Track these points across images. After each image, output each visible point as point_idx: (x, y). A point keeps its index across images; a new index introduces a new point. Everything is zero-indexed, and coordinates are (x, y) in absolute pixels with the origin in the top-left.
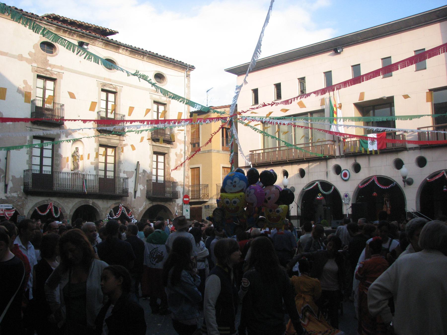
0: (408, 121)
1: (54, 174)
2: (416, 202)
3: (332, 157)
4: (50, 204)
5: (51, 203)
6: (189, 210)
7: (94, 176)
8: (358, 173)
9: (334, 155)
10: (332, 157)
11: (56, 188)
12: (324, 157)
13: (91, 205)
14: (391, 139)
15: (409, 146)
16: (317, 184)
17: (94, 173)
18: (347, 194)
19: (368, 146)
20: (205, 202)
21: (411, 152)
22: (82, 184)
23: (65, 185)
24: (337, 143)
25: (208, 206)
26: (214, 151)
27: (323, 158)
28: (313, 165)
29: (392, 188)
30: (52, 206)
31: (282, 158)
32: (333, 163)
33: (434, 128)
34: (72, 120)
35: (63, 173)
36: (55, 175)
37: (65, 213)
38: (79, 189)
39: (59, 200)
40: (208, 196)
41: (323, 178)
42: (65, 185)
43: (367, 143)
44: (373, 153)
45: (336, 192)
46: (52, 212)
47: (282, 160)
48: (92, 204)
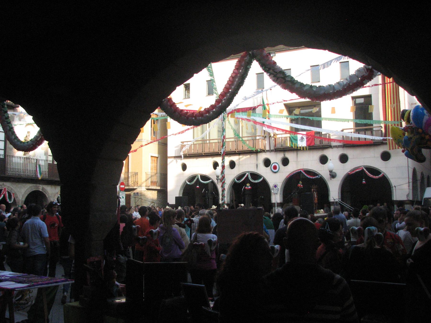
0: (346, 123)
1: (7, 158)
2: (339, 193)
3: (262, 151)
4: (4, 189)
5: (5, 189)
6: (124, 197)
7: (44, 161)
8: (288, 166)
9: (264, 149)
10: (263, 151)
11: (9, 173)
12: (255, 150)
13: (41, 190)
14: (319, 136)
15: (333, 144)
16: (247, 176)
17: (44, 158)
18: (277, 185)
19: (298, 142)
20: (134, 189)
21: (335, 149)
22: (35, 170)
23: (20, 170)
24: (267, 139)
25: (138, 193)
26: (144, 141)
27: (254, 151)
28: (243, 158)
29: (317, 179)
30: (6, 191)
31: (198, 150)
32: (263, 156)
33: (354, 130)
34: (267, 95)
35: (17, 157)
36: (8, 159)
37: (17, 199)
38: (32, 175)
39: (13, 185)
40: (137, 183)
41: (253, 169)
42: (20, 170)
43: (297, 140)
44: (302, 149)
45: (265, 183)
46: (6, 197)
47: (193, 154)
48: (42, 190)
